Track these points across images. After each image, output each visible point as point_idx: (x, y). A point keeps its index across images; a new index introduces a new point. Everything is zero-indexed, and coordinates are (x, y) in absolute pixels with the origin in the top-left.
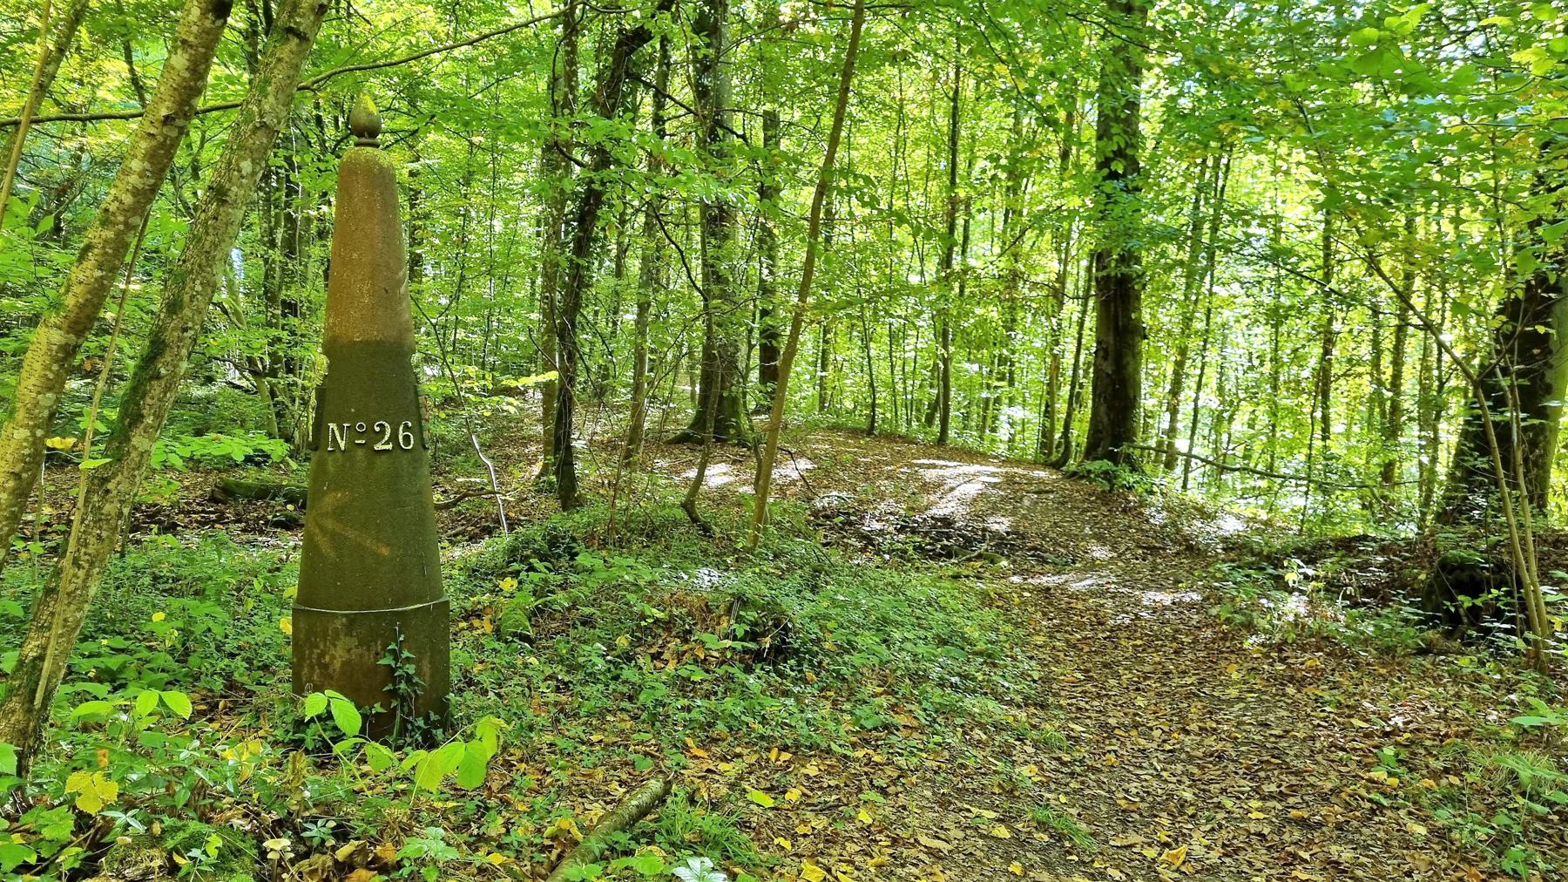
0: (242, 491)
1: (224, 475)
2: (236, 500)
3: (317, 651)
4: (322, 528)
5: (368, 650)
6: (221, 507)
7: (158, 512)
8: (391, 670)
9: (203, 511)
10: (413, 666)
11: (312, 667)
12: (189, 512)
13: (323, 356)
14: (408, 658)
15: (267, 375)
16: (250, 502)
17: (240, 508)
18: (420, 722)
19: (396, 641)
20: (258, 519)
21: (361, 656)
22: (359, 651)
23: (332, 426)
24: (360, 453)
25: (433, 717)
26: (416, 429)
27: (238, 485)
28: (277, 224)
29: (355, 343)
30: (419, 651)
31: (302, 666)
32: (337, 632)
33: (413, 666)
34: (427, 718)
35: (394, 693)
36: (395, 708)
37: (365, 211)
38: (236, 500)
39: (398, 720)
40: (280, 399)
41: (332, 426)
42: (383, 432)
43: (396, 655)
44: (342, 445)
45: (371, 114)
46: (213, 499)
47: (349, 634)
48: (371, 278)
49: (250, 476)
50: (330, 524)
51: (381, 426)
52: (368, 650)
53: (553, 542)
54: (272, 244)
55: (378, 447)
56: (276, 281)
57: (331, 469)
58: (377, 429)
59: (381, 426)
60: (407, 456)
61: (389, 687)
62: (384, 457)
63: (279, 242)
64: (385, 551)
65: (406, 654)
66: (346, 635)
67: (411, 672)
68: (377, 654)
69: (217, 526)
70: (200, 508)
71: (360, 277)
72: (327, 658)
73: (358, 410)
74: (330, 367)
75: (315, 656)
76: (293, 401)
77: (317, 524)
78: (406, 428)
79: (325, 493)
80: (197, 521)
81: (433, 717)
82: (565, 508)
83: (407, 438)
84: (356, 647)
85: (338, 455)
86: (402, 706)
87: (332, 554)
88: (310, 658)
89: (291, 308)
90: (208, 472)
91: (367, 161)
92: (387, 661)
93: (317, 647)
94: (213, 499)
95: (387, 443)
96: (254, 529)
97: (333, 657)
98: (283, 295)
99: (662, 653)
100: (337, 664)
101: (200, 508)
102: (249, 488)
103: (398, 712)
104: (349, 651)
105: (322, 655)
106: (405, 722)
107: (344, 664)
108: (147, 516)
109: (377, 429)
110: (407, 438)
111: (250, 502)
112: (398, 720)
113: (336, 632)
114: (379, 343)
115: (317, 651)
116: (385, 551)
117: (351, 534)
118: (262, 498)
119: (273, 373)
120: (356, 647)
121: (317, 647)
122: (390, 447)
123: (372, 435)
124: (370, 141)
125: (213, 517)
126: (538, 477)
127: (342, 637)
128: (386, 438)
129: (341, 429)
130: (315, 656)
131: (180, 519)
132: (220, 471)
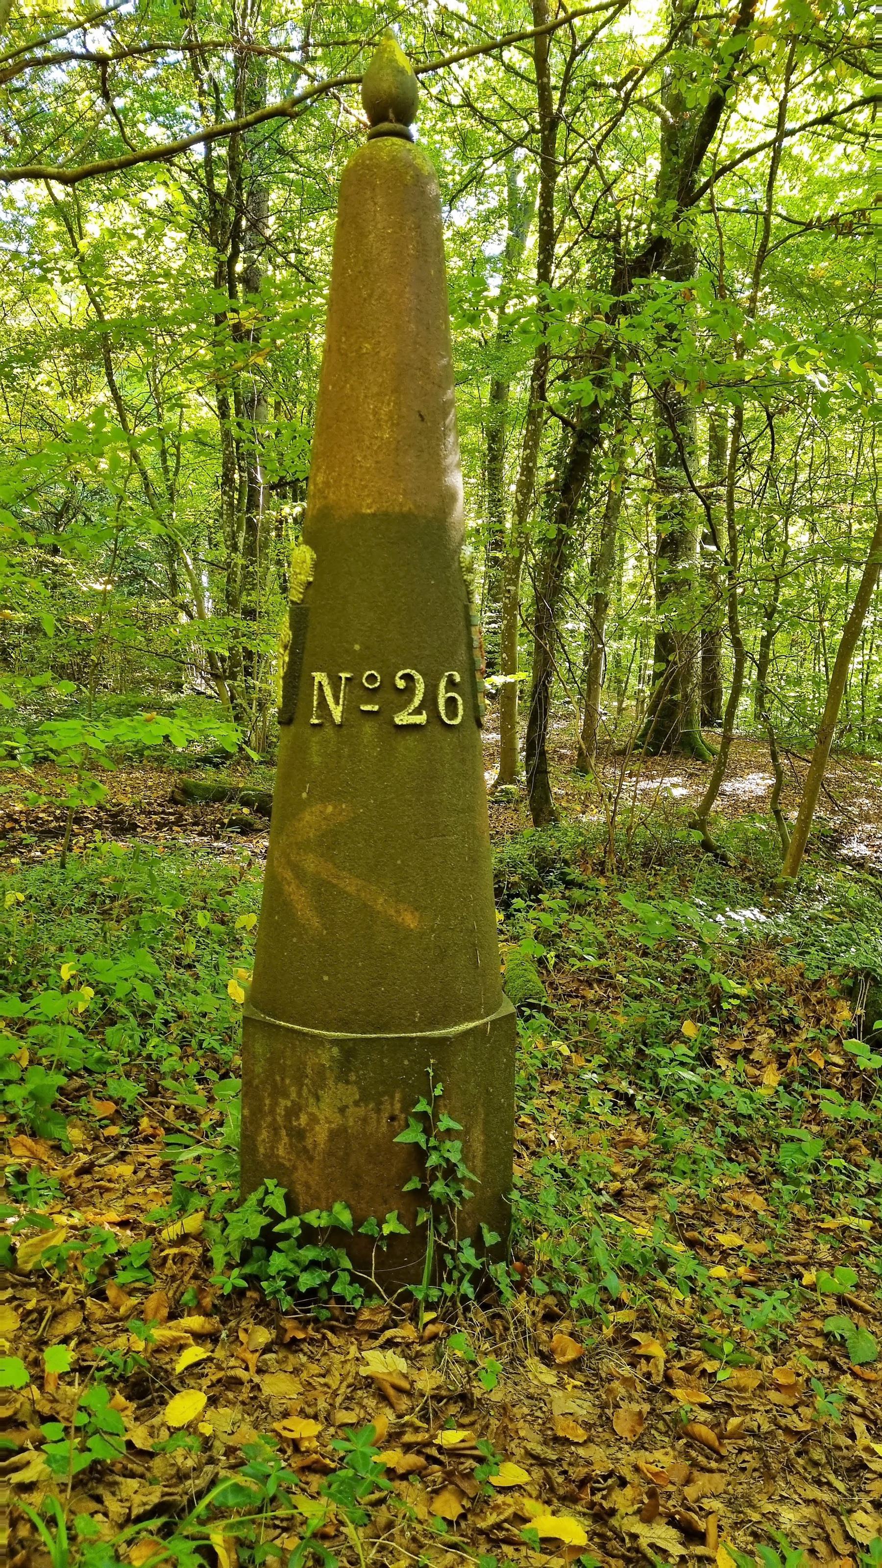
0: (200, 792)
1: (185, 777)
2: (194, 801)
3: (284, 1103)
4: (300, 874)
5: (378, 1111)
6: (180, 808)
7: (121, 812)
8: (419, 1154)
9: (163, 812)
10: (458, 1144)
11: (275, 1129)
12: (150, 813)
13: (305, 548)
14: (448, 1131)
15: (226, 678)
16: (207, 804)
17: (198, 810)
18: (468, 1256)
19: (428, 1094)
20: (215, 822)
21: (365, 1120)
22: (361, 1111)
23: (320, 677)
24: (369, 728)
25: (490, 1238)
26: (467, 688)
27: (197, 786)
28: (239, 528)
29: (364, 516)
30: (464, 1113)
31: (258, 1128)
32: (321, 1072)
33: (458, 1144)
34: (478, 1242)
35: (421, 1196)
36: (425, 1226)
37: (387, 258)
38: (194, 801)
39: (430, 1251)
40: (239, 701)
41: (320, 677)
42: (410, 690)
43: (427, 1123)
44: (337, 713)
45: (401, 71)
46: (173, 801)
47: (343, 1077)
48: (395, 391)
49: (207, 777)
50: (311, 863)
51: (408, 678)
52: (378, 1111)
53: (544, 865)
54: (235, 548)
55: (403, 718)
56: (237, 586)
57: (316, 760)
58: (401, 684)
59: (408, 678)
60: (450, 737)
61: (413, 1184)
62: (411, 740)
63: (241, 546)
64: (410, 920)
65: (446, 1122)
66: (338, 1079)
67: (455, 1158)
68: (393, 1118)
69: (175, 828)
70: (160, 809)
71: (375, 389)
72: (303, 1119)
73: (366, 647)
74: (317, 566)
75: (280, 1111)
76: (250, 705)
77: (289, 863)
78: (452, 684)
79: (303, 805)
80: (157, 823)
81: (490, 1238)
82: (537, 823)
83: (451, 702)
84: (356, 1104)
85: (329, 731)
86: (437, 1220)
87: (316, 922)
88: (272, 1111)
89: (250, 613)
90: (170, 773)
91: (394, 159)
92: (412, 1135)
93: (286, 1095)
94: (173, 801)
95: (418, 711)
96: (210, 834)
97: (314, 1119)
98: (244, 599)
99: (750, 1051)
100: (321, 1134)
101: (160, 809)
102: (207, 789)
103: (430, 1233)
104: (342, 1110)
105: (293, 1112)
106: (440, 1250)
107: (334, 1135)
108: (111, 816)
109: (401, 684)
110: (451, 702)
111: (207, 804)
112: (430, 1251)
113: (321, 1072)
114: (405, 518)
115: (285, 1103)
116: (410, 920)
117: (350, 885)
118: (220, 800)
119: (233, 676)
120: (356, 1104)
121: (286, 1095)
122: (421, 719)
123: (392, 696)
124: (399, 127)
125: (172, 818)
126: (495, 786)
127: (330, 1082)
128: (417, 702)
129: (335, 683)
130: (280, 1111)
131: (141, 820)
132: (181, 772)
